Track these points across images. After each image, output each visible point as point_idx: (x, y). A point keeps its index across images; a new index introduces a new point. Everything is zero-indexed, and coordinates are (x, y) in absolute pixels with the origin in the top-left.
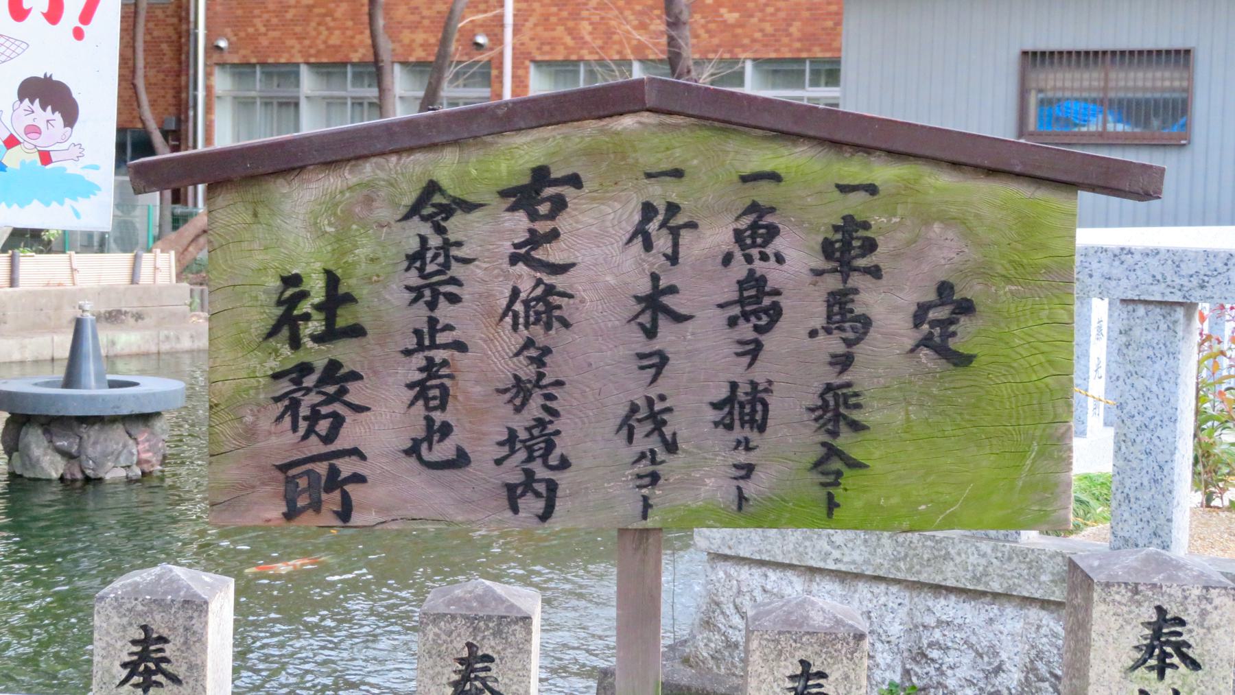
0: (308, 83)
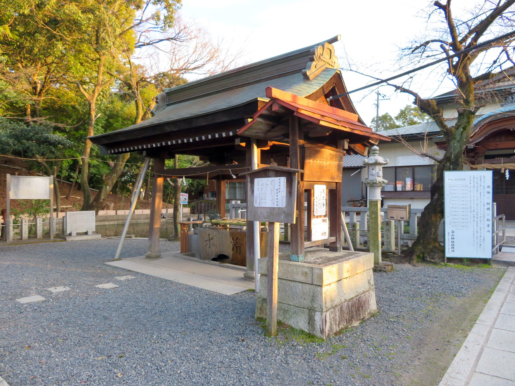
0: (237, 185)
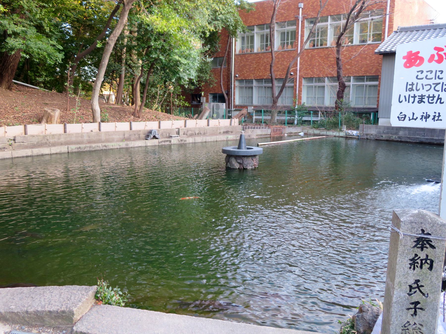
0: (255, 83)
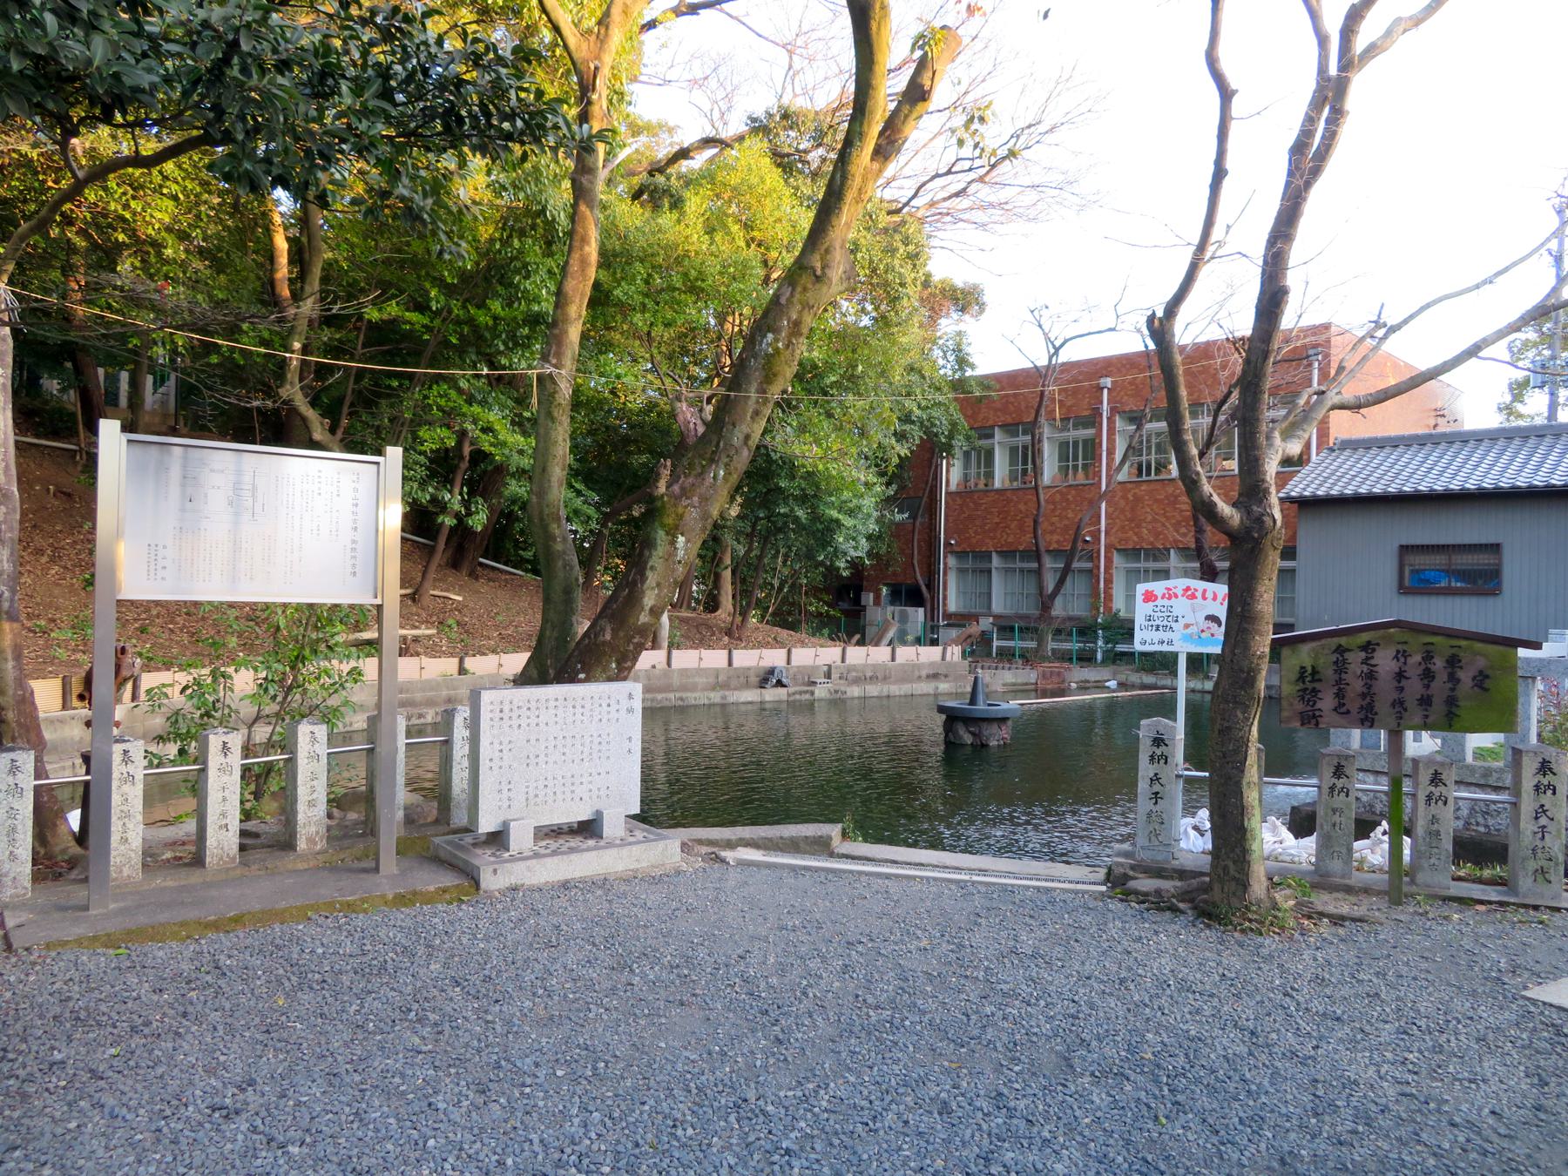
0: (996, 561)
